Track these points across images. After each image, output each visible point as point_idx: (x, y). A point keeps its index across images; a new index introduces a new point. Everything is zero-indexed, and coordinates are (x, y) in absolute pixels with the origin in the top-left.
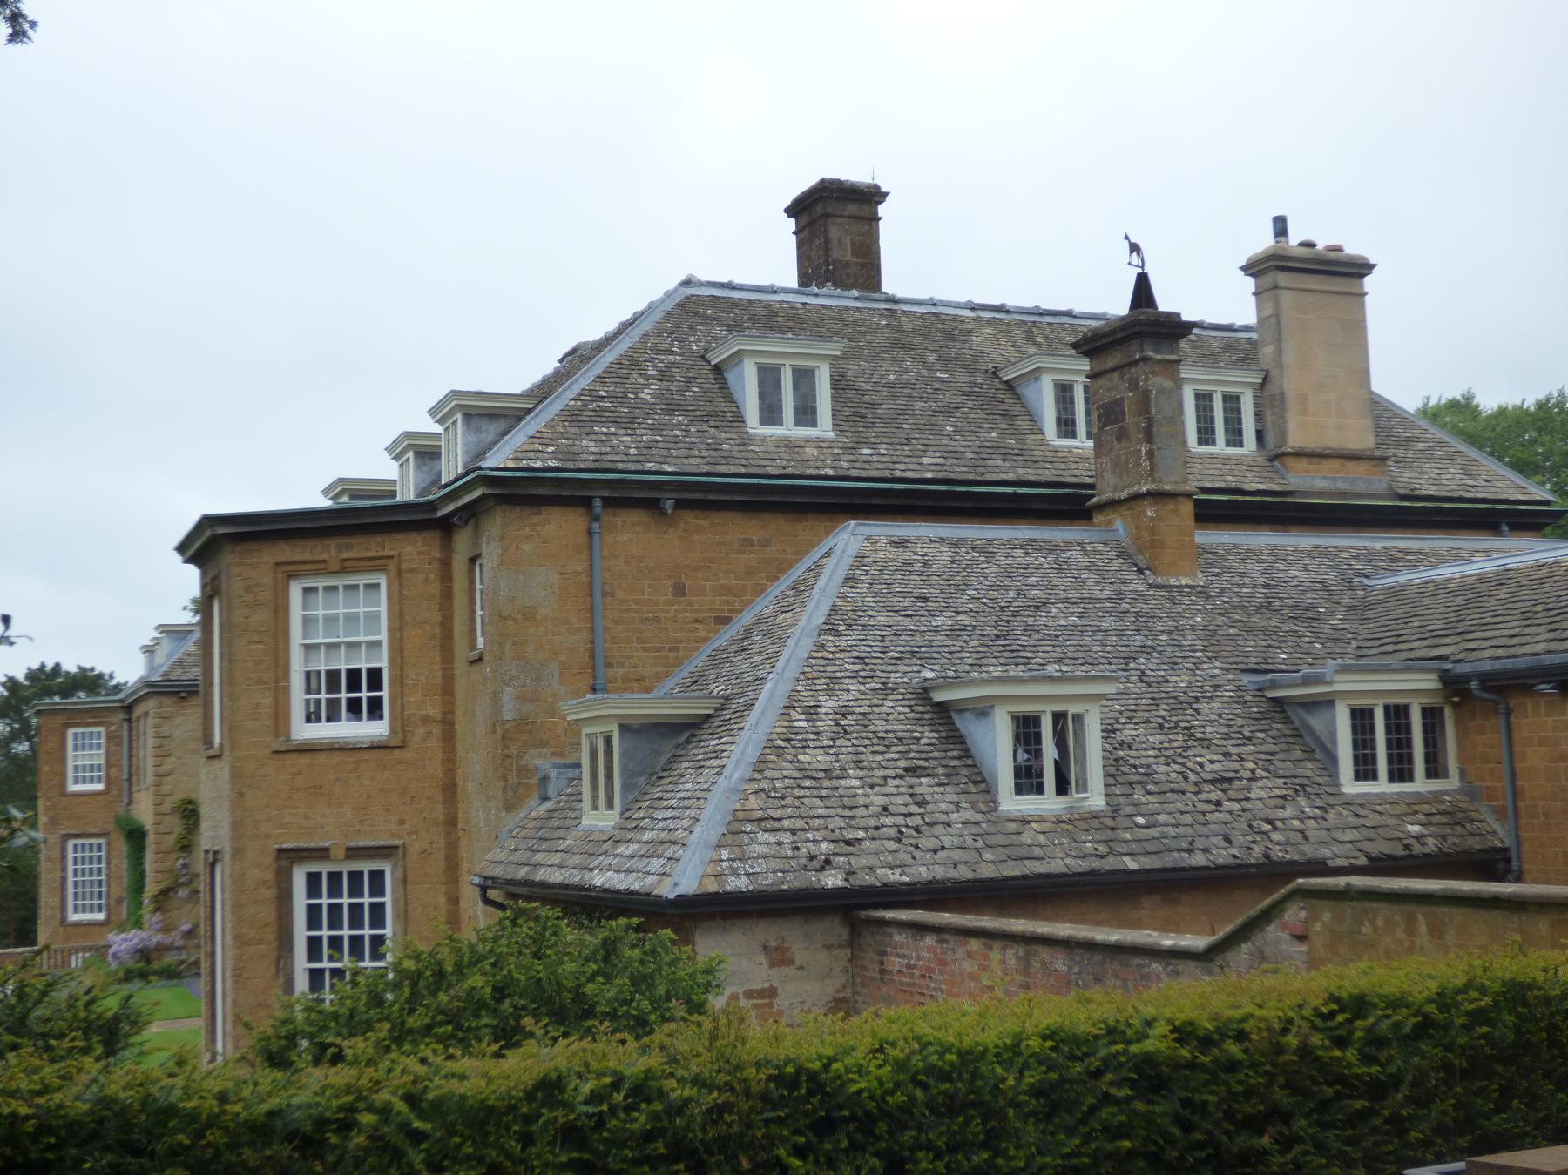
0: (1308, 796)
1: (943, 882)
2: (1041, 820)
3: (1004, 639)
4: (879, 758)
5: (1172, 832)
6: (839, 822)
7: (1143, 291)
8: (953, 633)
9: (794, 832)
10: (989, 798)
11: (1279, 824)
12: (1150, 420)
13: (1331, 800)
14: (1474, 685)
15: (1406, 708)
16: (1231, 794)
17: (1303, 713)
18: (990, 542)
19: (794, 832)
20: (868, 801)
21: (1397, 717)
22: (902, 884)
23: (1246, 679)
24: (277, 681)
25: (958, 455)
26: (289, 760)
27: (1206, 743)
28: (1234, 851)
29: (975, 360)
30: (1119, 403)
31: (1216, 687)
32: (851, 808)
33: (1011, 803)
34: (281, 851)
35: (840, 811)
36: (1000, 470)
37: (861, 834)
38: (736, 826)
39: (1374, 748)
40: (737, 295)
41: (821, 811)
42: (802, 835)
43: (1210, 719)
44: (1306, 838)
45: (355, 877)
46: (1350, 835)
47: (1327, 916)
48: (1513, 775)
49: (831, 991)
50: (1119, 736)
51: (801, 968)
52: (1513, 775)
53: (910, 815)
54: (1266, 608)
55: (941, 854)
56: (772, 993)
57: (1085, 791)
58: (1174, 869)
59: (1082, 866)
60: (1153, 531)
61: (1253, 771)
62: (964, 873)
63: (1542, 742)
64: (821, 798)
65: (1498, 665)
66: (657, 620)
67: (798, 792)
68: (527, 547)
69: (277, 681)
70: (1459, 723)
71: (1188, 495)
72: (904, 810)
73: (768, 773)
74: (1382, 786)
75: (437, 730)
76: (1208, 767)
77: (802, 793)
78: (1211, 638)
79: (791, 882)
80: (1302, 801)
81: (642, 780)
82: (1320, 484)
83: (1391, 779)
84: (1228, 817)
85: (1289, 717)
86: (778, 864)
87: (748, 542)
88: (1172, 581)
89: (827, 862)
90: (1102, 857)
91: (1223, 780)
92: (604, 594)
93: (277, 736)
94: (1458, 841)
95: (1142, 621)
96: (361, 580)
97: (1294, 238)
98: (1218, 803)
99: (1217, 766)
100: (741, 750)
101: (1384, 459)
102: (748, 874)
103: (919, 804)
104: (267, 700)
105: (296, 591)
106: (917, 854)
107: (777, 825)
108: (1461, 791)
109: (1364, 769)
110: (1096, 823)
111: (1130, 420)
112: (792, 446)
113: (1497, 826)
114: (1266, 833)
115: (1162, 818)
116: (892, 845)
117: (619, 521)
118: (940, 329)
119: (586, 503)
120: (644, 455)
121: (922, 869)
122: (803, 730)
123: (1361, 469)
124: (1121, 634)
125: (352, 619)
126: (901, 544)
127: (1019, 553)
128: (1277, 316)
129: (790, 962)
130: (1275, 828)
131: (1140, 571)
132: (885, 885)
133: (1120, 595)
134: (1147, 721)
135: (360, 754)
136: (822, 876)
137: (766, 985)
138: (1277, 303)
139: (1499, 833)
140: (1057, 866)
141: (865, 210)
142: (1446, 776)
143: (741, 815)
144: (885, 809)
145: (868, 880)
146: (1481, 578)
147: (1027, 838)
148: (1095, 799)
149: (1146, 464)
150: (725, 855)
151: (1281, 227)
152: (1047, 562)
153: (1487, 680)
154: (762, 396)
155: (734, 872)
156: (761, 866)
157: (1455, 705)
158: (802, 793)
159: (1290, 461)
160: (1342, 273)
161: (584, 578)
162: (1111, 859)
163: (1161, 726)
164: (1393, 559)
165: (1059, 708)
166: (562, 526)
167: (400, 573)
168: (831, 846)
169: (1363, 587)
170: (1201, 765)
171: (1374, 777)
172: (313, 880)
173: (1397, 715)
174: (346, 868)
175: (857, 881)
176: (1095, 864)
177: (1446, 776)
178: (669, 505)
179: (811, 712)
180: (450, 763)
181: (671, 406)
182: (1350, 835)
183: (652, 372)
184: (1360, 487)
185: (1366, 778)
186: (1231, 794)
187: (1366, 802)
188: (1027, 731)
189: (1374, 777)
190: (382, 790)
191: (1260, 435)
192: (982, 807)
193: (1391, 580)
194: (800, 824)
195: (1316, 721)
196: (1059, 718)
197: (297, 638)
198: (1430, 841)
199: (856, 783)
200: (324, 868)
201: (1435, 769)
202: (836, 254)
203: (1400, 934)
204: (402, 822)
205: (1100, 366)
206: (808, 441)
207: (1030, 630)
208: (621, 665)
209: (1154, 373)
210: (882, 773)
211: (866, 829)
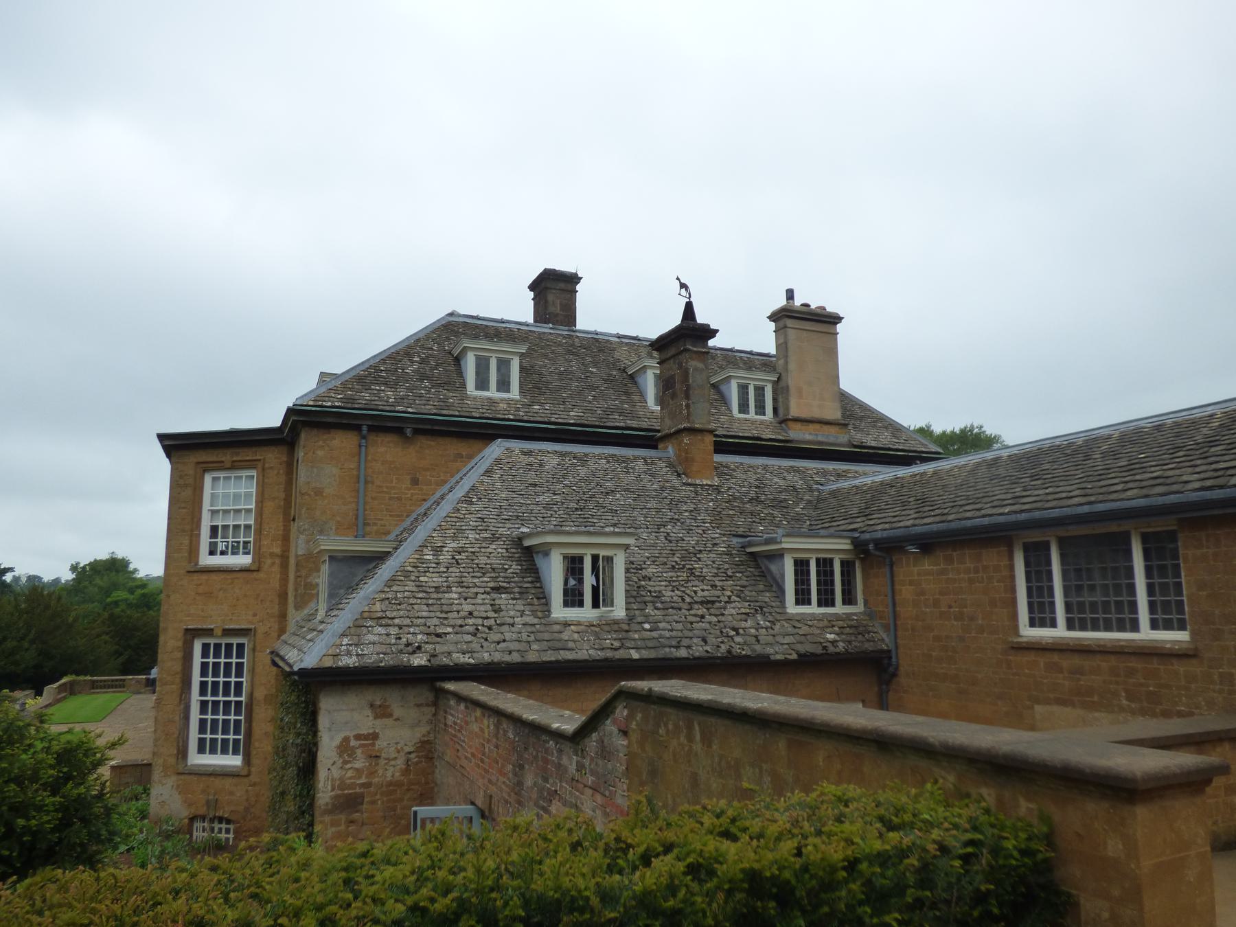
0: (763, 614)
1: (499, 663)
2: (579, 624)
3: (581, 512)
4: (476, 580)
5: (667, 634)
6: (436, 621)
7: (689, 310)
8: (548, 506)
9: (400, 627)
10: (545, 608)
11: (741, 631)
12: (688, 387)
13: (778, 617)
14: (871, 547)
15: (831, 560)
16: (712, 611)
17: (767, 562)
18: (586, 455)
19: (400, 627)
20: (460, 608)
21: (825, 565)
22: (469, 664)
23: (735, 540)
24: (192, 531)
25: (592, 412)
26: (196, 576)
27: (702, 578)
28: (708, 648)
29: (614, 363)
30: (673, 377)
31: (715, 545)
32: (447, 613)
33: (559, 612)
34: (187, 630)
35: (438, 614)
36: (617, 420)
37: (449, 630)
38: (360, 622)
39: (809, 585)
40: (480, 322)
41: (424, 614)
42: (406, 629)
43: (706, 565)
44: (758, 641)
45: (229, 646)
46: (788, 640)
47: (639, 716)
48: (894, 604)
49: (419, 735)
50: (644, 572)
51: (397, 719)
52: (894, 604)
53: (487, 618)
54: (756, 500)
55: (503, 645)
56: (375, 736)
57: (612, 605)
58: (663, 659)
59: (601, 655)
60: (687, 452)
61: (729, 597)
62: (516, 658)
63: (911, 583)
64: (428, 605)
65: (885, 534)
66: (399, 499)
67: (411, 601)
68: (320, 453)
69: (192, 531)
70: (863, 571)
71: (711, 432)
72: (484, 615)
73: (395, 588)
74: (813, 609)
75: (278, 561)
76: (700, 593)
77: (414, 601)
78: (717, 517)
79: (388, 661)
80: (759, 617)
81: (342, 591)
82: (808, 437)
83: (820, 605)
84: (708, 626)
85: (758, 563)
86: (379, 648)
87: (460, 456)
88: (698, 482)
89: (419, 648)
90: (616, 649)
91: (708, 602)
92: (366, 482)
93: (190, 562)
94: (858, 645)
95: (674, 504)
96: (244, 473)
97: (798, 301)
98: (703, 617)
99: (706, 593)
100: (386, 570)
101: (846, 425)
102: (358, 655)
103: (495, 612)
104: (187, 542)
105: (208, 479)
106: (485, 644)
107: (390, 622)
108: (864, 613)
109: (802, 597)
110: (616, 627)
111: (677, 386)
112: (492, 402)
113: (885, 636)
114: (732, 637)
115: (661, 625)
116: (469, 638)
117: (379, 439)
118: (599, 345)
119: (357, 428)
120: (397, 403)
121: (486, 655)
122: (429, 561)
123: (833, 430)
124: (658, 511)
125: (226, 496)
126: (529, 453)
127: (604, 461)
128: (786, 343)
129: (390, 715)
130: (738, 634)
131: (679, 475)
132: (456, 665)
133: (663, 488)
134: (665, 564)
135: (236, 575)
136: (411, 658)
137: (371, 731)
138: (786, 336)
139: (884, 639)
140: (582, 655)
141: (569, 287)
142: (856, 604)
143: (366, 615)
144: (471, 613)
145: (445, 661)
146: (882, 483)
147: (565, 636)
148: (619, 611)
149: (685, 412)
150: (345, 641)
151: (790, 294)
152: (620, 468)
153: (878, 543)
154: (477, 373)
155: (349, 654)
156: (373, 649)
157: (862, 560)
158: (414, 601)
159: (790, 423)
160: (826, 321)
161: (355, 472)
162: (621, 651)
163: (673, 567)
164: (839, 475)
165: (595, 552)
166: (342, 442)
167: (264, 469)
168: (425, 638)
169: (818, 490)
170: (695, 592)
171: (809, 603)
172: (205, 647)
173: (825, 565)
174: (224, 641)
175: (435, 662)
176: (609, 654)
177: (856, 604)
178: (409, 432)
179: (437, 550)
180: (284, 580)
181: (422, 376)
182: (788, 640)
183: (416, 359)
184: (832, 440)
185: (803, 604)
186: (712, 611)
187: (801, 619)
188: (574, 566)
189: (809, 603)
190: (245, 596)
191: (775, 410)
192: (540, 614)
193: (834, 487)
194: (407, 622)
195: (773, 568)
196: (595, 558)
197: (206, 505)
198: (841, 644)
199: (455, 596)
200: (212, 641)
201: (849, 599)
202: (551, 309)
203: (683, 739)
204: (255, 615)
205: (665, 356)
206: (502, 400)
207: (599, 506)
208: (375, 524)
209: (692, 359)
210: (475, 590)
211: (453, 626)
